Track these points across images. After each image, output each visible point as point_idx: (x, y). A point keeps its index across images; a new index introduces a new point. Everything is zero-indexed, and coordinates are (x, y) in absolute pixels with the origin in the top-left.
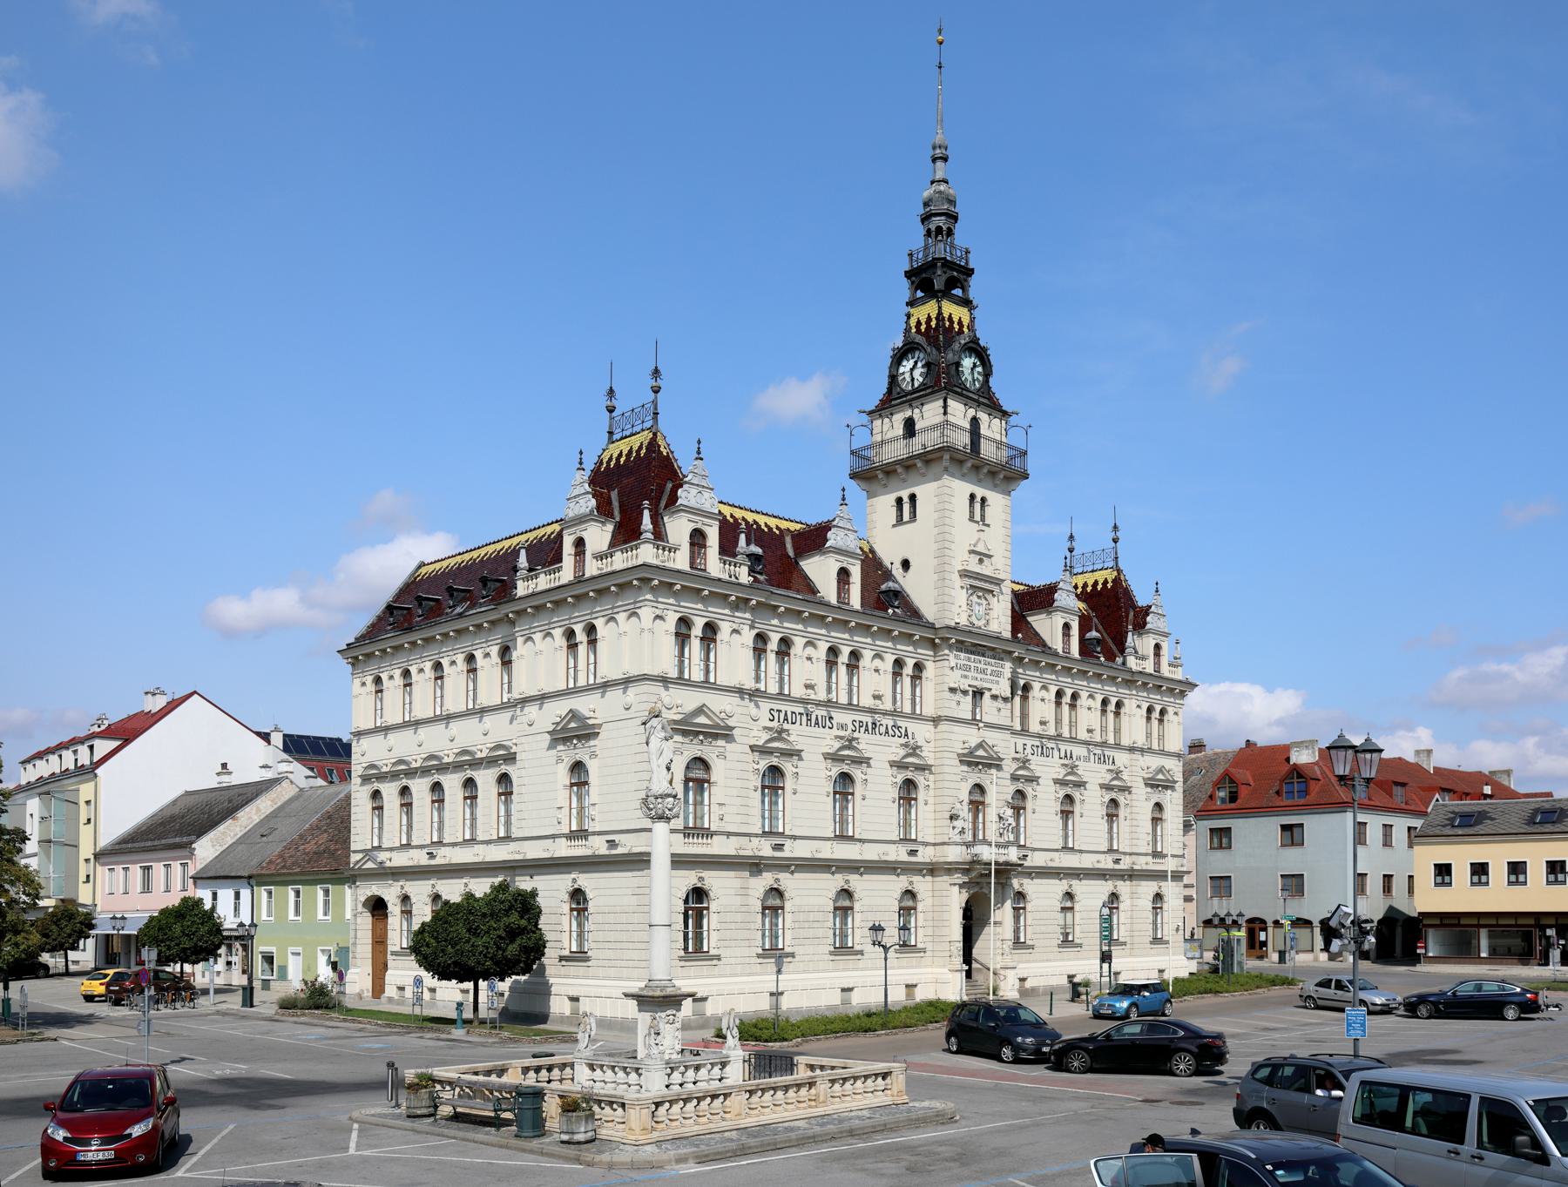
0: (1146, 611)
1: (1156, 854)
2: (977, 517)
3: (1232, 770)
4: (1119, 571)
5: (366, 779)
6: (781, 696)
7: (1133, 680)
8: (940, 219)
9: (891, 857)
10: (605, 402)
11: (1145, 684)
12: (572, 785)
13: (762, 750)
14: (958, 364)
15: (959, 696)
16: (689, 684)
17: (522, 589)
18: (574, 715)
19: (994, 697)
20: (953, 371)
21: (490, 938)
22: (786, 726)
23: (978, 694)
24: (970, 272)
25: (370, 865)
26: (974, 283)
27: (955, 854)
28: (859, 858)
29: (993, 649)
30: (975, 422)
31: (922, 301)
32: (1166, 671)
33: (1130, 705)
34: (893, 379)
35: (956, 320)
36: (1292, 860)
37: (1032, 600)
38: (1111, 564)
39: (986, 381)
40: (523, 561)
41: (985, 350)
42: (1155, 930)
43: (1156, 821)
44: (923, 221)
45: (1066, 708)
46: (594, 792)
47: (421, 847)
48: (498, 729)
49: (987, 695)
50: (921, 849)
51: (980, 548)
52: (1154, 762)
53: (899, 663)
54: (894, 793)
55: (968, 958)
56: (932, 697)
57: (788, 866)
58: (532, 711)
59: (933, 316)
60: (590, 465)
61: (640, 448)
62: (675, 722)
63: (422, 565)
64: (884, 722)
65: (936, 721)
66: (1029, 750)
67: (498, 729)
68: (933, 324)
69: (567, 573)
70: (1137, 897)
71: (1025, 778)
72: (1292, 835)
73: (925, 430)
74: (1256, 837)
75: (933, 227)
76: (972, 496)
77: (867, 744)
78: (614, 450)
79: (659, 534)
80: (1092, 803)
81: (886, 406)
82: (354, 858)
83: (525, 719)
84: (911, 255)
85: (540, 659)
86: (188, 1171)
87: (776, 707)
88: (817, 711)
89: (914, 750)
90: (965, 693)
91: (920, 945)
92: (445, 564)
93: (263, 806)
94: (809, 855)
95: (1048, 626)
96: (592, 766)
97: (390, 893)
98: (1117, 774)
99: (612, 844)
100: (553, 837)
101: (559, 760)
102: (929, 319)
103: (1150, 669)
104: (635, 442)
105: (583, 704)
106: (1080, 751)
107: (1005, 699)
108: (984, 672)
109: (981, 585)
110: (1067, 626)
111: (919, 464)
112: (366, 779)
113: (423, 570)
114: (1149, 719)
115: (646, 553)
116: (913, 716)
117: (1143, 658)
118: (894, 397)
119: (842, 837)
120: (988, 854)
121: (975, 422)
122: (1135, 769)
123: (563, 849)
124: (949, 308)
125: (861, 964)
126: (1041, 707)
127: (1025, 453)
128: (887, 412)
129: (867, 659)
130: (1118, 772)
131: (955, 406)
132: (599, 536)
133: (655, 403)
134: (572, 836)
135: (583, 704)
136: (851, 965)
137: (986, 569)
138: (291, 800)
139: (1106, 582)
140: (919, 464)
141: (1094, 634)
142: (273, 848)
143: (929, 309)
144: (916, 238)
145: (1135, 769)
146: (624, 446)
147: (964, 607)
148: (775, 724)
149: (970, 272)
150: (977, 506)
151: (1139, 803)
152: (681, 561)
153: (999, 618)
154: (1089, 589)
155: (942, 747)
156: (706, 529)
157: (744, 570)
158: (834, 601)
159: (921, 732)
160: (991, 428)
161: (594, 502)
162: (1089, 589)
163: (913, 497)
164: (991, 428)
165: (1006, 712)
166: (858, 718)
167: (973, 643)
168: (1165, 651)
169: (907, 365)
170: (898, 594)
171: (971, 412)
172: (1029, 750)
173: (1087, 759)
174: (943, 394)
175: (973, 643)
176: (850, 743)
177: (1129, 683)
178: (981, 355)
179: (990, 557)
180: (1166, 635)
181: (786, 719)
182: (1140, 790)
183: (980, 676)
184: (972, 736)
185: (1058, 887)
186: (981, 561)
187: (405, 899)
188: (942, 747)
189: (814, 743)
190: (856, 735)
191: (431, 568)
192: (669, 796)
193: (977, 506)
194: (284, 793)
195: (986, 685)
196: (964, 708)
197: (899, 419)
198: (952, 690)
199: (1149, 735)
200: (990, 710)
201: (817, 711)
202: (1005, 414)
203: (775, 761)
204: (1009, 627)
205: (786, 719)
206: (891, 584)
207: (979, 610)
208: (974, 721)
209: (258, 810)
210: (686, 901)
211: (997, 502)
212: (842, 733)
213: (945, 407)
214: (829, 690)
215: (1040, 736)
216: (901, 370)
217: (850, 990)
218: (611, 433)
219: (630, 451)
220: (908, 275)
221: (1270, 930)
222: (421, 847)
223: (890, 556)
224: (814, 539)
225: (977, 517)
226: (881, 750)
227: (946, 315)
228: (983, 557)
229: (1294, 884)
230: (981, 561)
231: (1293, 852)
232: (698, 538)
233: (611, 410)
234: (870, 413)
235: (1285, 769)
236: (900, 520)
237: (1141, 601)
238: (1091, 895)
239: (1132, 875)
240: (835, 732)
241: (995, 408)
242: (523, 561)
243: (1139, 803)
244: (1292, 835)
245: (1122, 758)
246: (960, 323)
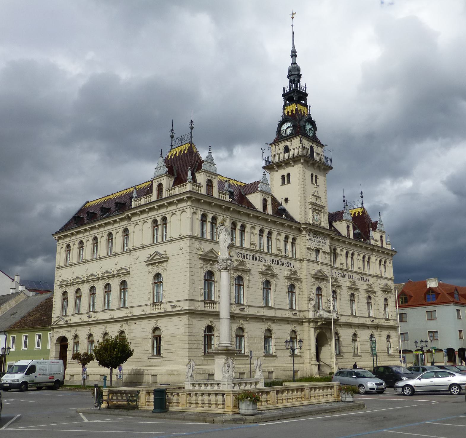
0: (376, 223)
1: (387, 319)
2: (314, 182)
3: (404, 290)
4: (364, 209)
5: (61, 286)
6: (241, 247)
7: (373, 249)
8: (295, 74)
9: (287, 316)
10: (170, 134)
11: (378, 251)
12: (155, 283)
13: (236, 269)
14: (305, 126)
15: (311, 252)
16: (207, 240)
17: (134, 205)
18: (156, 253)
19: (324, 252)
20: (303, 129)
21: (114, 353)
22: (244, 260)
23: (318, 251)
24: (307, 95)
25: (61, 322)
26: (308, 98)
27: (311, 315)
28: (274, 315)
29: (323, 233)
30: (312, 147)
31: (289, 105)
32: (385, 246)
33: (373, 259)
34: (279, 131)
35: (302, 111)
36: (432, 326)
37: (335, 217)
38: (361, 206)
39: (315, 133)
40: (135, 194)
41: (314, 122)
42: (388, 350)
43: (386, 305)
44: (288, 77)
45: (349, 259)
46: (165, 286)
47: (85, 314)
48: (123, 262)
49: (321, 251)
50: (298, 313)
51: (316, 194)
52: (384, 282)
53: (287, 237)
54: (286, 290)
55: (318, 359)
56: (301, 250)
57: (246, 318)
58: (138, 253)
59: (294, 109)
60: (165, 156)
61: (185, 150)
62: (201, 255)
63: (88, 202)
64: (282, 260)
65: (301, 260)
66: (337, 275)
67: (123, 262)
68: (294, 112)
69: (154, 196)
70: (380, 336)
71: (336, 286)
72: (431, 316)
73: (292, 149)
74: (417, 315)
75: (292, 79)
76: (312, 175)
77: (276, 269)
78: (173, 152)
79: (194, 180)
80: (362, 296)
81: (276, 142)
82: (53, 320)
83: (135, 257)
84: (284, 89)
85: (141, 231)
86: (8, 427)
87: (240, 252)
88: (256, 254)
89: (294, 272)
90: (313, 250)
91: (298, 354)
92: (98, 201)
93: (12, 303)
94: (254, 314)
95: (341, 227)
96: (163, 274)
97: (69, 334)
98: (370, 286)
99: (173, 307)
100: (146, 305)
101: (150, 273)
102: (292, 111)
103: (380, 245)
104: (183, 148)
105: (161, 249)
106: (356, 276)
107: (328, 253)
108: (319, 242)
109: (317, 208)
110: (348, 227)
111: (291, 162)
112: (61, 286)
113: (88, 204)
114: (380, 264)
115: (189, 187)
116: (293, 258)
117: (377, 241)
118: (280, 138)
119: (267, 307)
120: (325, 315)
121: (312, 147)
122: (377, 285)
123: (149, 310)
124: (300, 107)
125: (276, 361)
126: (341, 259)
127: (331, 160)
128: (277, 144)
129: (274, 235)
130: (371, 285)
131: (305, 142)
132: (167, 182)
133: (191, 133)
134: (154, 304)
135: (161, 249)
136: (272, 362)
137: (318, 202)
138: (23, 301)
139: (359, 213)
140: (291, 162)
141: (357, 231)
142: (15, 319)
143: (293, 107)
144: (286, 83)
145: (377, 285)
146: (178, 150)
147: (311, 216)
148: (240, 259)
149: (307, 95)
150: (314, 179)
151: (379, 297)
152: (203, 191)
153: (324, 222)
154: (356, 215)
155: (305, 271)
156: (213, 179)
157: (227, 197)
158: (262, 211)
159: (296, 265)
160: (317, 150)
161: (167, 169)
162: (356, 215)
163: (289, 175)
164: (317, 150)
165: (328, 259)
166: (272, 258)
167: (314, 230)
168: (384, 238)
169: (284, 127)
170: (284, 211)
171: (311, 144)
172: (337, 275)
173: (358, 279)
174: (300, 136)
175: (314, 230)
176: (270, 268)
177: (373, 250)
178: (313, 123)
179: (320, 198)
180: (384, 232)
181: (244, 257)
182: (380, 293)
183: (318, 244)
184: (318, 268)
185: (351, 331)
186: (316, 199)
187: (76, 337)
188: (305, 271)
189: (256, 267)
190: (271, 265)
191: (92, 203)
192: (229, 259)
193: (314, 179)
194: (22, 297)
195: (321, 247)
196: (313, 257)
197: (282, 145)
198: (308, 248)
199: (381, 271)
200: (322, 258)
201: (256, 254)
202: (322, 146)
203: (240, 274)
204: (328, 225)
205: (244, 257)
206: (282, 207)
207: (317, 218)
208: (316, 262)
209: (10, 305)
210: (205, 332)
211: (321, 179)
212: (266, 264)
213: (301, 141)
214: (260, 247)
215: (341, 269)
216: (282, 129)
217: (272, 372)
218: (172, 146)
219: (181, 152)
220: (283, 96)
221: (425, 354)
222: (85, 314)
223: (280, 198)
224: (253, 188)
225: (314, 182)
226: (282, 272)
227: (299, 109)
228: (317, 197)
229: (433, 334)
230: (316, 199)
231: (432, 322)
232: (209, 183)
233: (172, 137)
234: (270, 144)
235: (426, 290)
236: (283, 183)
237: (373, 220)
238: (364, 335)
239: (377, 327)
240: (263, 263)
241: (319, 143)
242: (135, 194)
243: (379, 297)
244: (431, 316)
245: (372, 280)
246: (304, 112)
